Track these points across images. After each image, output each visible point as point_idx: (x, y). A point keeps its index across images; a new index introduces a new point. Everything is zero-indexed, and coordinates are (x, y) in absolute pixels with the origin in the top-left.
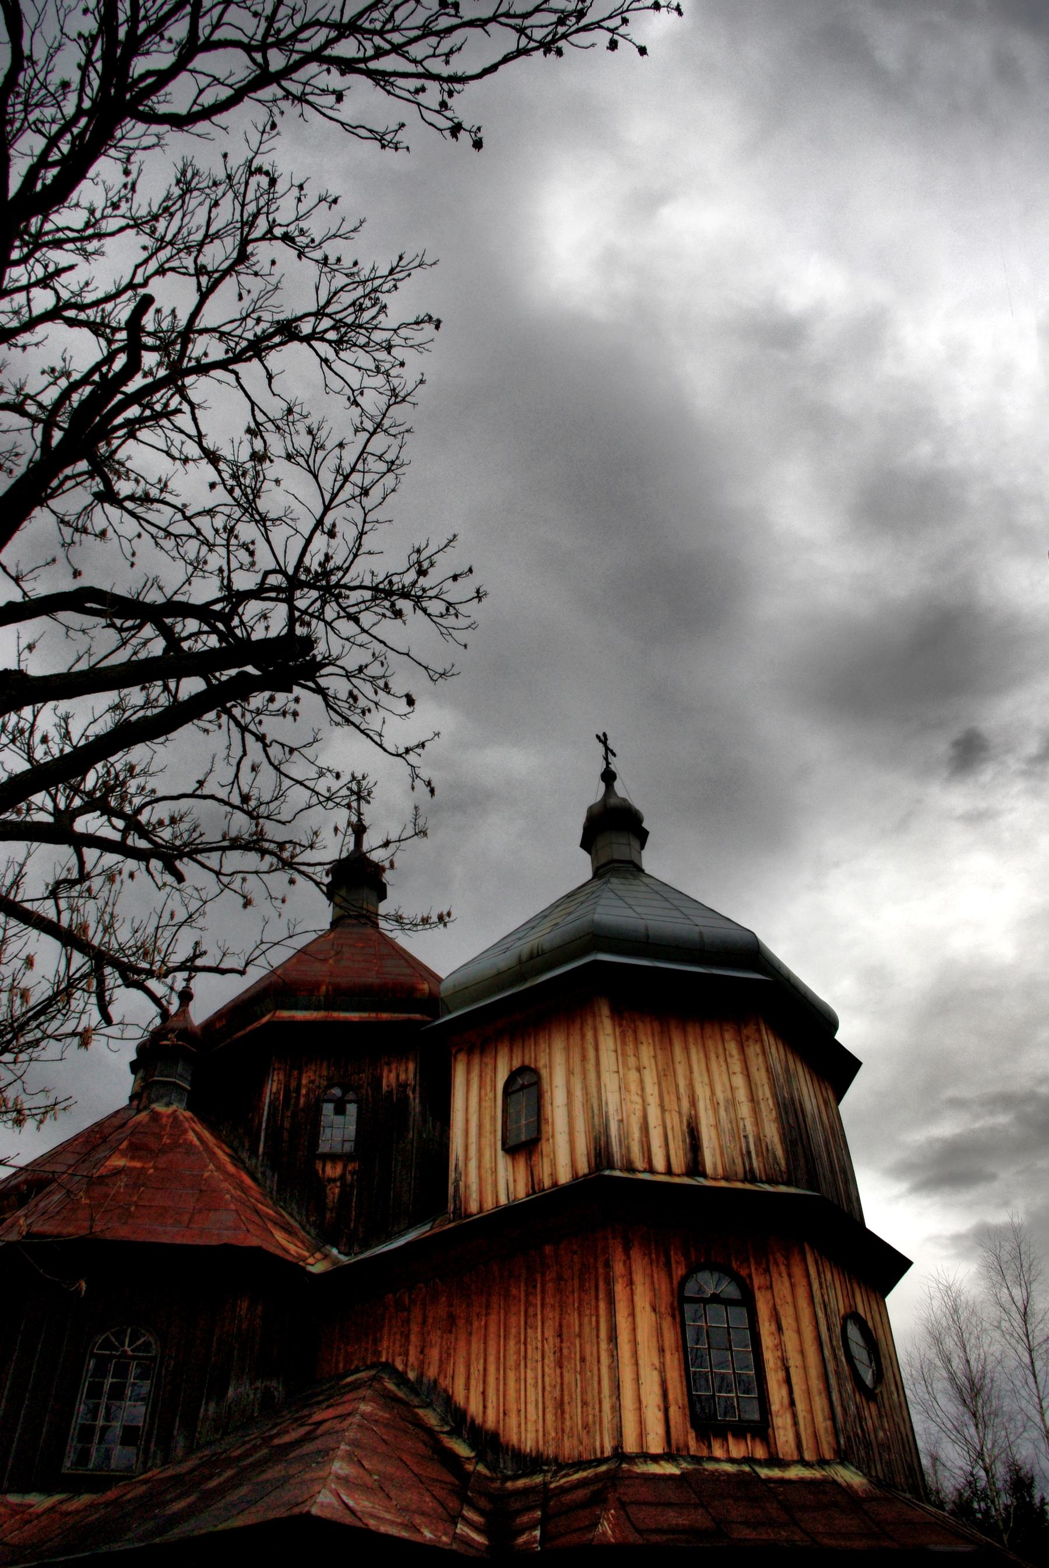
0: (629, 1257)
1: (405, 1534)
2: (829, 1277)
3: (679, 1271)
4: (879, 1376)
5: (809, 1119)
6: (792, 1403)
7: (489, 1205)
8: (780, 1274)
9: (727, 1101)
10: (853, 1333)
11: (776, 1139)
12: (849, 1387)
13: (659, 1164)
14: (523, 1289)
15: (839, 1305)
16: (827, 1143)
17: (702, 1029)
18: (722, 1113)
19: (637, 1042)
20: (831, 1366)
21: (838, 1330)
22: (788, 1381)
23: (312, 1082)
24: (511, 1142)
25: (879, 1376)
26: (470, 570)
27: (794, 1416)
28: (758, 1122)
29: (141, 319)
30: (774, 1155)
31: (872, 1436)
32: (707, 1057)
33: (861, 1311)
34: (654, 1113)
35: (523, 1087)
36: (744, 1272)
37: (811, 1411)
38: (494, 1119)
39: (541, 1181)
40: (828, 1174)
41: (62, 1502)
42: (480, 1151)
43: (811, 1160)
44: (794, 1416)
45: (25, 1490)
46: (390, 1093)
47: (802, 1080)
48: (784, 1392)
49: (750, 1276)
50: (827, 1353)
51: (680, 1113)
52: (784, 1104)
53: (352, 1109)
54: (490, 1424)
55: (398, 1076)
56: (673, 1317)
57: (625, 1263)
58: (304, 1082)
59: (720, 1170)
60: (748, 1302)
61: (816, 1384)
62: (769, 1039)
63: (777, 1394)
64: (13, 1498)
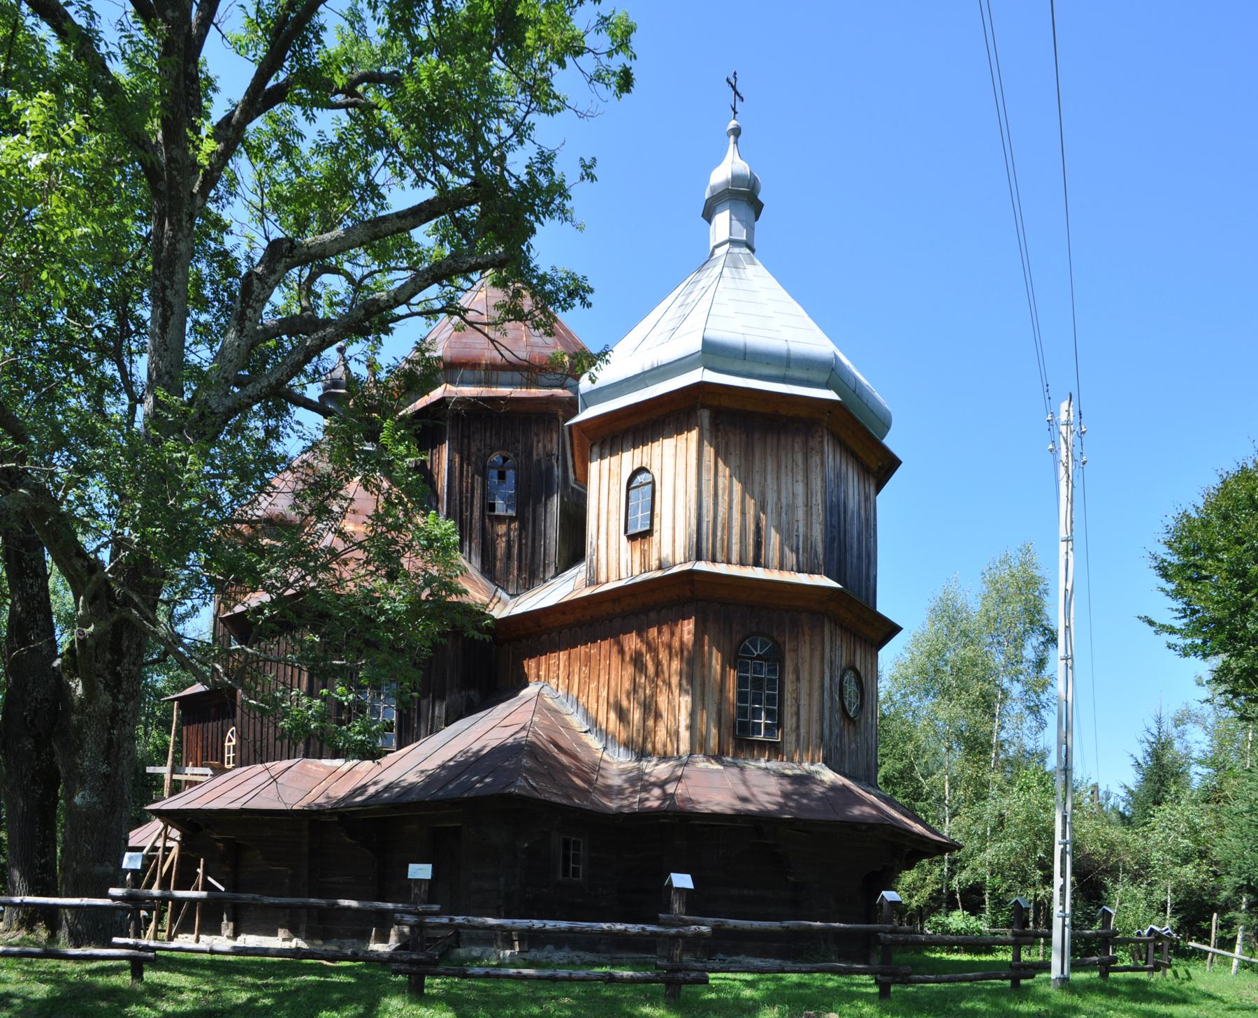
1: (564, 802)
2: (838, 643)
4: (861, 706)
5: (850, 513)
6: (798, 727)
9: (788, 505)
11: (819, 539)
12: (837, 716)
15: (842, 659)
16: (860, 534)
17: (779, 440)
18: (784, 515)
20: (827, 705)
21: (837, 680)
22: (798, 714)
23: (479, 450)
24: (630, 532)
25: (861, 706)
27: (798, 736)
28: (809, 525)
32: (779, 467)
37: (808, 733)
40: (855, 560)
46: (539, 461)
47: (850, 483)
48: (794, 720)
50: (826, 696)
52: (831, 508)
53: (510, 474)
55: (544, 447)
58: (473, 450)
61: (815, 716)
62: (828, 449)
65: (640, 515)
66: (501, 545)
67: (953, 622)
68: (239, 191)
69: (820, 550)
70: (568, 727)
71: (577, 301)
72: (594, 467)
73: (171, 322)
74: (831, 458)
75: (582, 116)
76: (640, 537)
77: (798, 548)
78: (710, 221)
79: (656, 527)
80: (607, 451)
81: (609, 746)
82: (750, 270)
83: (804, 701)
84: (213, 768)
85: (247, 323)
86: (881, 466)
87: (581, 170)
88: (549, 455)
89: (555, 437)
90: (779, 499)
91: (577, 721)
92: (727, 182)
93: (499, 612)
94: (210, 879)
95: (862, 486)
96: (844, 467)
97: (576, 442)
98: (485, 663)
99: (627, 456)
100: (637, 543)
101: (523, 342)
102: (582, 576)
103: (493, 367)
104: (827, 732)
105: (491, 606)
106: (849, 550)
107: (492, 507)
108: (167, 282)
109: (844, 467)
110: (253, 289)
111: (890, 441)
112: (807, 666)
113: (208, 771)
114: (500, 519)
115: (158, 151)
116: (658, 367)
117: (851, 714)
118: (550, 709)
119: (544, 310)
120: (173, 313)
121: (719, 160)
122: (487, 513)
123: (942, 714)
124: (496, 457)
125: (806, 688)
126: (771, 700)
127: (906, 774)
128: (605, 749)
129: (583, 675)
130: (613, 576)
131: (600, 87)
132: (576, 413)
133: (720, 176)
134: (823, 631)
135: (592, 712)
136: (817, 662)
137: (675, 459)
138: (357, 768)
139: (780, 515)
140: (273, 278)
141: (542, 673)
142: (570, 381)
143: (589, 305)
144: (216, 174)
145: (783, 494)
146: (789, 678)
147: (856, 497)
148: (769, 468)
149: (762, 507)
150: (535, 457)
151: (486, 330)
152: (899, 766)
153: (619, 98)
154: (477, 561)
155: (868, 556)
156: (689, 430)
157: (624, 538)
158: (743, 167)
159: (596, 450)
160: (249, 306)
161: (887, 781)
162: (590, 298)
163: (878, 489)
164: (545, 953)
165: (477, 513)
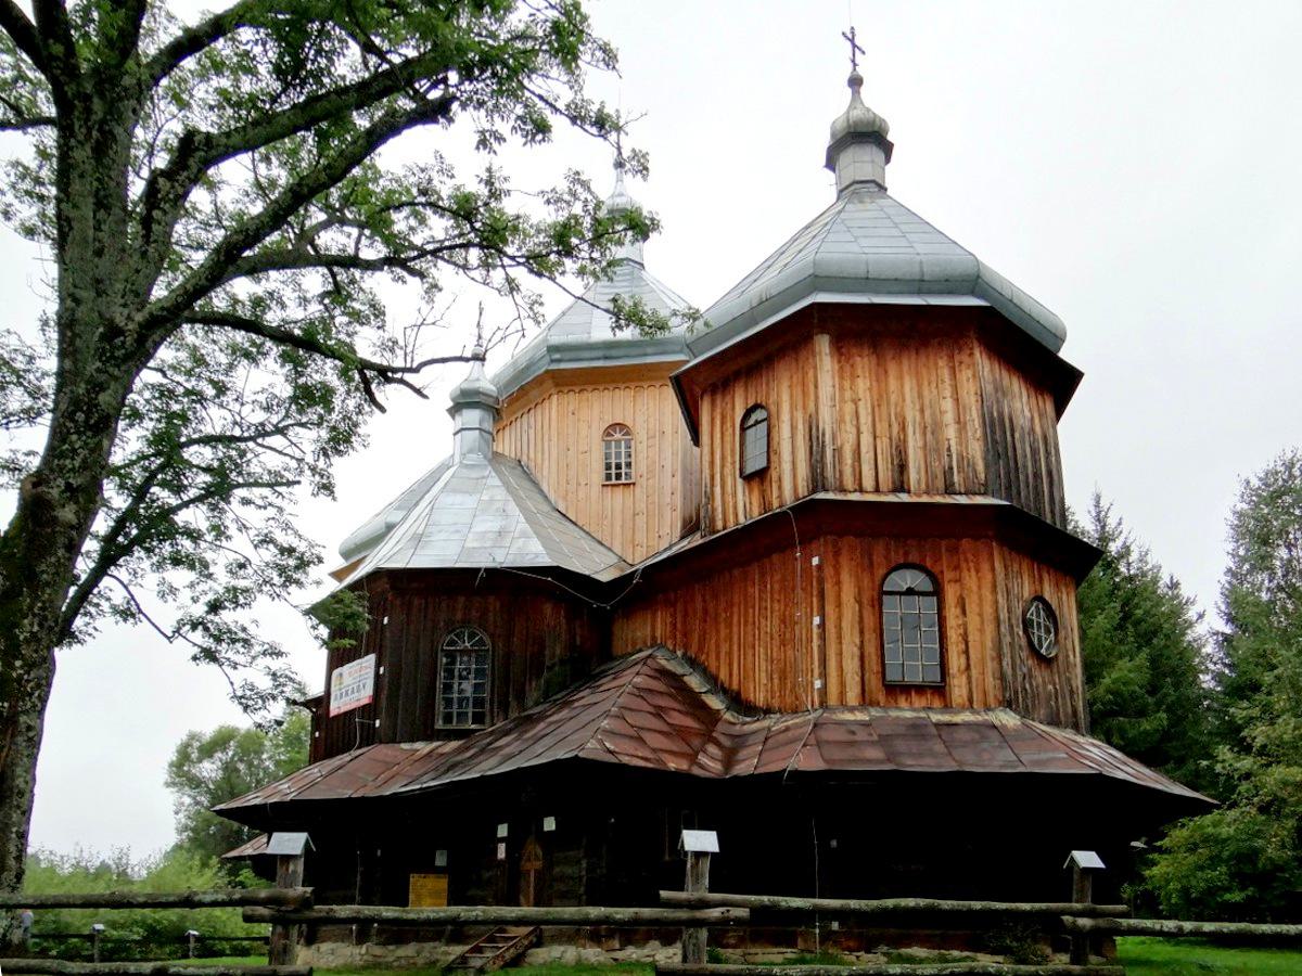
0: (837, 562)
3: (882, 572)
6: (968, 667)
7: (731, 527)
8: (969, 570)
12: (1024, 654)
13: (868, 483)
14: (757, 587)
16: (1035, 452)
19: (854, 377)
24: (749, 470)
27: (969, 678)
29: (70, 626)
30: (975, 471)
31: (1041, 689)
32: (920, 386)
33: (1047, 596)
34: (866, 439)
36: (936, 570)
38: (733, 451)
39: (771, 504)
41: (437, 748)
42: (722, 479)
43: (1013, 470)
44: (969, 678)
45: (412, 740)
48: (963, 660)
49: (942, 572)
51: (890, 439)
54: (735, 686)
56: (873, 606)
57: (834, 566)
59: (923, 486)
60: (938, 592)
64: (405, 746)
69: (980, 467)
73: (70, 239)
79: (773, 465)
85: (155, 227)
86: (887, 149)
95: (1033, 400)
111: (1066, 354)
112: (975, 597)
134: (992, 555)
136: (987, 593)
139: (925, 434)
157: (740, 481)
164: (646, 951)
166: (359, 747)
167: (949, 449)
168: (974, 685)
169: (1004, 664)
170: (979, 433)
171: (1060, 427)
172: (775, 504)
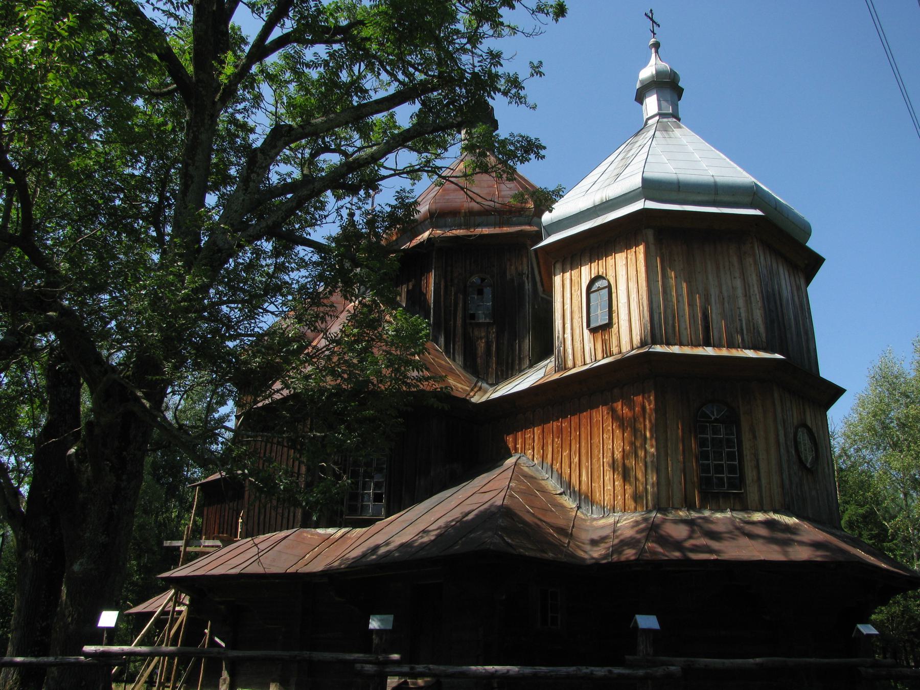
4: (817, 457)
6: (759, 479)
10: (803, 437)
18: (726, 305)
21: (791, 436)
22: (757, 467)
24: (593, 325)
25: (817, 457)
26: (534, 108)
27: (760, 487)
28: (750, 311)
30: (758, 332)
33: (809, 423)
35: (599, 289)
44: (760, 487)
48: (755, 473)
50: (782, 450)
53: (488, 291)
55: (516, 269)
63: (750, 474)
64: (321, 531)
65: (599, 312)
66: (481, 345)
67: (893, 386)
68: (262, 105)
69: (762, 329)
70: (543, 491)
71: (532, 156)
72: (557, 279)
73: (191, 188)
74: (763, 258)
75: (528, 35)
76: (602, 330)
77: (742, 329)
78: (642, 103)
79: (615, 320)
80: (568, 266)
81: (583, 505)
82: (677, 132)
83: (762, 456)
84: (222, 540)
85: (251, 184)
87: (530, 70)
88: (521, 274)
89: (525, 260)
90: (721, 292)
91: (552, 485)
92: (653, 76)
93: (477, 399)
94: (217, 639)
95: (792, 278)
96: (775, 265)
97: (541, 264)
98: (473, 440)
99: (585, 269)
100: (599, 335)
101: (491, 190)
102: (552, 365)
103: (471, 213)
104: (787, 482)
105: (472, 394)
106: (791, 332)
107: (473, 317)
108: (190, 161)
109: (775, 265)
110: (259, 160)
111: (812, 244)
113: (218, 543)
114: (479, 325)
115: (204, 82)
116: (607, 201)
117: (808, 465)
118: (526, 476)
119: (504, 163)
120: (192, 182)
121: (645, 64)
122: (468, 321)
123: (896, 464)
124: (475, 279)
125: (763, 445)
126: (731, 456)
127: (869, 518)
128: (579, 508)
129: (556, 446)
130: (579, 362)
131: (541, 16)
132: (541, 240)
133: (647, 72)
135: (566, 477)
137: (627, 271)
138: (349, 535)
140: (273, 151)
141: (519, 446)
142: (535, 219)
143: (543, 157)
144: (233, 88)
145: (724, 288)
146: (746, 437)
147: (789, 288)
148: (710, 277)
149: (707, 299)
150: (508, 277)
151: (277, 33)
152: (861, 511)
153: (557, 21)
154: (460, 359)
155: (806, 333)
156: (637, 245)
157: (586, 332)
158: (665, 66)
159: (558, 266)
160: (253, 172)
161: (851, 524)
162: (542, 152)
163: (808, 282)
165: (459, 322)
166: (140, 644)
167: (740, 316)
168: (764, 490)
169: (784, 476)
170: (760, 304)
171: (810, 289)
172: (615, 350)
